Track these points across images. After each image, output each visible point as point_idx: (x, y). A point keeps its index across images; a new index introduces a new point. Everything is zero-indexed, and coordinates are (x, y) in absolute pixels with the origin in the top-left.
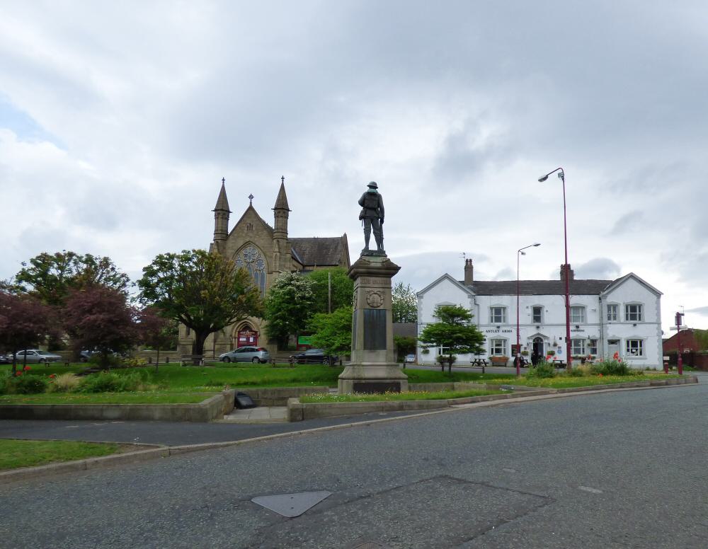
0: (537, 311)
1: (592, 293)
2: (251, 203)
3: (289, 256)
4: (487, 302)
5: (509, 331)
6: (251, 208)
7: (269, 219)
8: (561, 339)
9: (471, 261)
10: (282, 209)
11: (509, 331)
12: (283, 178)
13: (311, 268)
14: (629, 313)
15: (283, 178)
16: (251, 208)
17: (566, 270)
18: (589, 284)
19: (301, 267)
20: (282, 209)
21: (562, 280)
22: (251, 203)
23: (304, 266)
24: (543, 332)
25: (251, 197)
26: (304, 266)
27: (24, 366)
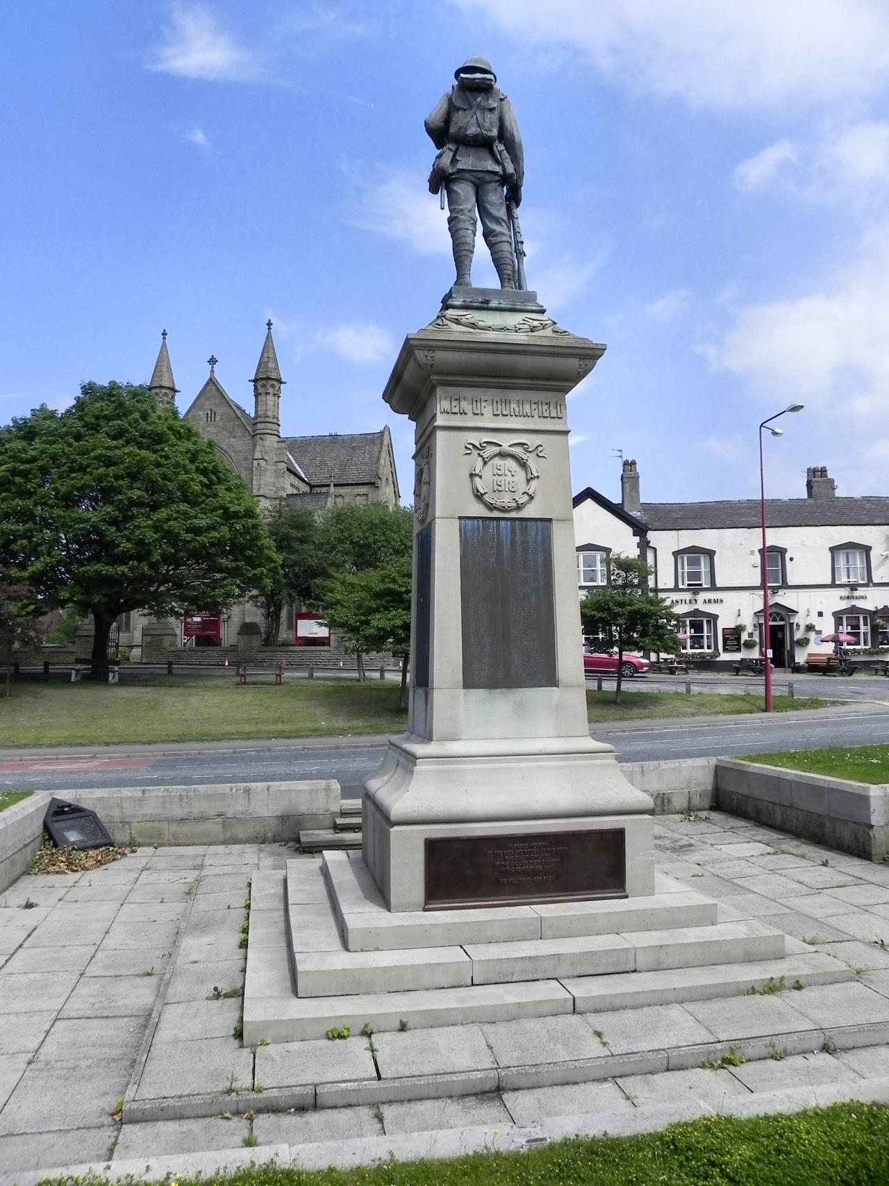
0: (773, 558)
1: (877, 521)
2: (212, 371)
3: (283, 466)
4: (665, 542)
5: (716, 601)
6: (212, 382)
7: (243, 396)
8: (820, 614)
9: (634, 463)
10: (266, 382)
11: (716, 601)
12: (164, 334)
13: (324, 490)
14: (582, 568)
15: (164, 334)
16: (212, 382)
17: (817, 478)
18: (868, 506)
19: (307, 489)
20: (266, 382)
21: (417, 508)
22: (212, 371)
23: (312, 487)
24: (786, 599)
25: (213, 361)
26: (312, 487)
27: (619, 686)
